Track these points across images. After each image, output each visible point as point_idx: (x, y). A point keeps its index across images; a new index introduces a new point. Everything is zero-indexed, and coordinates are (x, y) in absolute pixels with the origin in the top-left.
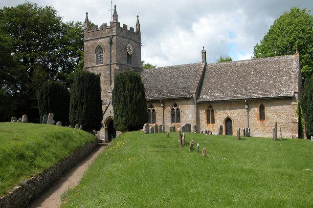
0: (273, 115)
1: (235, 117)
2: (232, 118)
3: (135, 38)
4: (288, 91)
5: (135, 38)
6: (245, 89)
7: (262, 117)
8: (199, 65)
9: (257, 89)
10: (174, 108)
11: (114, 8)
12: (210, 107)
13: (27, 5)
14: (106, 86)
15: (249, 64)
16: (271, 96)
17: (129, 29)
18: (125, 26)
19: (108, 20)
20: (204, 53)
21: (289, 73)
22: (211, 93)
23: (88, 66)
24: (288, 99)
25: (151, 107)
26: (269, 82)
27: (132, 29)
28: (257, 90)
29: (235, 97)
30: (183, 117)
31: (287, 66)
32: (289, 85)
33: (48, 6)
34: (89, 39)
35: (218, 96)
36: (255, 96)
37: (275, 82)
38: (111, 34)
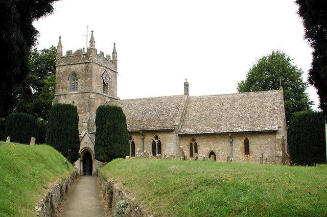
2: (216, 152)
5: (112, 66)
18: (102, 53)
19: (83, 45)
23: (61, 93)
24: (273, 133)
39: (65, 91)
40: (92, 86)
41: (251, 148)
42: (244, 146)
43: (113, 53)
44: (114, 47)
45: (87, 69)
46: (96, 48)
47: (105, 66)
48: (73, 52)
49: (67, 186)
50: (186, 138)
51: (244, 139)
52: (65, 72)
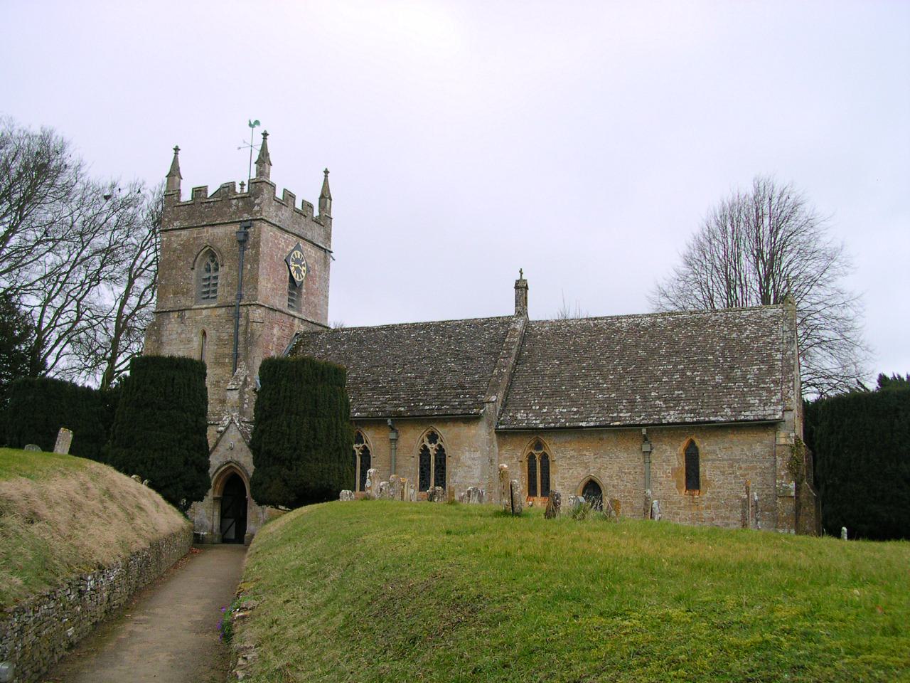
1: (611, 477)
2: (604, 481)
3: (316, 234)
4: (765, 404)
5: (316, 234)
6: (644, 398)
7: (693, 479)
8: (506, 322)
10: (429, 446)
11: (259, 140)
12: (539, 446)
14: (219, 371)
15: (654, 325)
17: (299, 205)
18: (289, 196)
19: (241, 173)
20: (521, 288)
21: (770, 355)
25: (359, 439)
28: (678, 400)
29: (613, 419)
30: (456, 474)
31: (762, 336)
32: (768, 390)
33: (66, 140)
34: (177, 224)
35: (561, 413)
36: (672, 417)
37: (728, 378)
38: (246, 216)
39: (184, 302)
42: (683, 465)
46: (272, 179)
47: (297, 232)
51: (684, 443)
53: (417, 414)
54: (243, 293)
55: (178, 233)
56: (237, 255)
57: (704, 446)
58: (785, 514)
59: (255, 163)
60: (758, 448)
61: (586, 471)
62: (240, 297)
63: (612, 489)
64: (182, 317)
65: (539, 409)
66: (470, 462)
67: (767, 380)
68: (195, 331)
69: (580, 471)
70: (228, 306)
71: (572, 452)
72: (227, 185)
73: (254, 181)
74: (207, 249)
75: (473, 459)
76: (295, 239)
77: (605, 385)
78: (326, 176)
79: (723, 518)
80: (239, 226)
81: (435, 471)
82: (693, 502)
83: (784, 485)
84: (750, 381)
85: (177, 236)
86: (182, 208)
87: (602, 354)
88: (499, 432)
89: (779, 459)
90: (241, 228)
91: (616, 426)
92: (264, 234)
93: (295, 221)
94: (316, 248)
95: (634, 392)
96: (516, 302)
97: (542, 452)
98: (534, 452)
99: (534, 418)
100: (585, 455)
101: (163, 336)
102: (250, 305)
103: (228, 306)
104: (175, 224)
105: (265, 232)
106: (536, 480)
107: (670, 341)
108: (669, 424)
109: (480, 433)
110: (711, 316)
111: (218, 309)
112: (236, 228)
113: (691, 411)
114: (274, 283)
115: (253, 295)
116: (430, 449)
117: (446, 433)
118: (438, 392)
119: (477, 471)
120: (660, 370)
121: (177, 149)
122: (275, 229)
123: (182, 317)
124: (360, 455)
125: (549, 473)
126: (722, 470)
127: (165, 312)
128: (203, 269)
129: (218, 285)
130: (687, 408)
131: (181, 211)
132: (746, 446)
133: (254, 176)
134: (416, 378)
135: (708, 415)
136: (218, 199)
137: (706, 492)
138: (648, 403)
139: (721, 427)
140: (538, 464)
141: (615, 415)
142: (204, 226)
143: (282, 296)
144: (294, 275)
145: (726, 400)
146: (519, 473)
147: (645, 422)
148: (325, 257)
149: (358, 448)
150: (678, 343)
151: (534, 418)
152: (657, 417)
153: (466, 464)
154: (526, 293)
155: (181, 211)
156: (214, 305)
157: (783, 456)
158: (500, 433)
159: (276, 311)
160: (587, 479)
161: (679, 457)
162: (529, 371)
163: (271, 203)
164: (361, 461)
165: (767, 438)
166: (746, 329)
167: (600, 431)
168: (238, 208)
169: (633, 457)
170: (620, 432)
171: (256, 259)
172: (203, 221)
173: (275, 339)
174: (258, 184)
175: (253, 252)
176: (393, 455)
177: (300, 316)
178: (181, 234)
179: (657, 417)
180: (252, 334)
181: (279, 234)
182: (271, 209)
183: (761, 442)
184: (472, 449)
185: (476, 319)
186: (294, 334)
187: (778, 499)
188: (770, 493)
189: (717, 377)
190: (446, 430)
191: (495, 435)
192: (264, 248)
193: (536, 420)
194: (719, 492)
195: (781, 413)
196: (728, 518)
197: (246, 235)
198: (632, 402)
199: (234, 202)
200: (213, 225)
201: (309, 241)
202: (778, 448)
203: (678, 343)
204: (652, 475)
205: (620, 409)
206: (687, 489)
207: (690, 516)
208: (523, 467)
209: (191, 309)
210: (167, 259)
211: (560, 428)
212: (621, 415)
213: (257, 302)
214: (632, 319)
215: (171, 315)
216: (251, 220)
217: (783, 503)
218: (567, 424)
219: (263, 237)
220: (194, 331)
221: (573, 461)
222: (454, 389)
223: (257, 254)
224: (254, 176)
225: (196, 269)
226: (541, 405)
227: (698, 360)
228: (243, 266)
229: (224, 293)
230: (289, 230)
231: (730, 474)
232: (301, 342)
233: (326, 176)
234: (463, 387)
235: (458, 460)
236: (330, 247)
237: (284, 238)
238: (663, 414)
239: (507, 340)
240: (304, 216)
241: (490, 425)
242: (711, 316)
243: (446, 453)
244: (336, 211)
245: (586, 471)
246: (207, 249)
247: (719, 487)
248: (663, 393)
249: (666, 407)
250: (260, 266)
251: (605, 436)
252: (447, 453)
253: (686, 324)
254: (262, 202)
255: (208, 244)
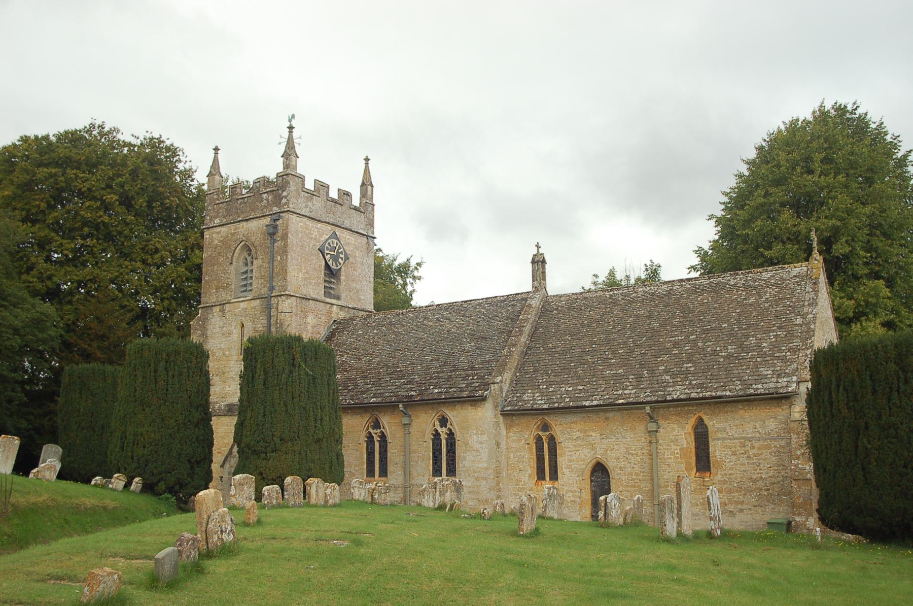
0: (734, 453)
1: (618, 459)
2: (610, 465)
3: (357, 222)
4: (779, 376)
5: (357, 222)
6: (652, 372)
8: (516, 302)
9: (687, 372)
10: (440, 430)
13: (805, 531)
16: (728, 393)
18: (320, 187)
19: (272, 168)
21: (790, 320)
22: (550, 384)
23: (213, 300)
24: (781, 398)
26: (726, 348)
27: (345, 194)
29: (620, 396)
32: (783, 359)
34: (217, 221)
35: (565, 393)
37: (742, 347)
38: (276, 209)
39: (224, 296)
40: (288, 279)
41: (717, 450)
42: (693, 445)
43: (363, 184)
44: (367, 171)
45: (272, 232)
46: (300, 170)
47: (332, 221)
48: (835, 341)
49: (532, 507)
50: (524, 420)
51: (692, 421)
52: (225, 242)
53: (426, 398)
54: (274, 284)
55: (218, 229)
56: (268, 247)
57: (713, 423)
58: (801, 499)
59: (282, 157)
60: (772, 425)
61: (593, 452)
62: (272, 288)
63: (619, 471)
64: (223, 311)
65: (546, 388)
66: (478, 446)
67: (784, 348)
68: (234, 324)
69: (586, 453)
70: (262, 298)
71: (578, 433)
72: (258, 180)
73: (281, 174)
74: (243, 243)
75: (481, 443)
76: (329, 228)
77: (614, 361)
78: (367, 164)
79: (737, 503)
80: (269, 219)
81: (447, 455)
82: (704, 485)
83: (800, 466)
84: (764, 350)
85: (218, 233)
86: (221, 205)
87: (614, 328)
88: (507, 415)
89: (794, 436)
90: (271, 220)
91: (622, 404)
92: (292, 225)
93: (329, 211)
94: (356, 235)
95: (642, 366)
96: (533, 277)
97: (548, 433)
98: (541, 433)
99: (540, 398)
100: (591, 436)
101: (207, 330)
102: (280, 296)
103: (262, 298)
104: (215, 222)
105: (293, 223)
106: (544, 463)
107: (685, 310)
108: (673, 400)
109: (486, 414)
110: (729, 280)
111: (253, 301)
112: (267, 221)
113: (700, 386)
114: (307, 273)
115: (282, 286)
116: (441, 433)
117: (454, 415)
118: (449, 374)
119: (484, 455)
120: (671, 341)
121: (216, 149)
122: (305, 219)
123: (223, 311)
124: (378, 440)
125: (556, 456)
126: (733, 449)
127: (209, 306)
128: (241, 263)
129: (253, 278)
130: (694, 382)
131: (221, 208)
132: (759, 422)
133: (281, 169)
134: (432, 361)
135: (716, 389)
136: (252, 194)
137: (716, 475)
138: (655, 378)
139: (730, 402)
140: (377, 445)
141: (620, 392)
142: (239, 221)
143: (317, 284)
144: (330, 263)
145: (737, 372)
146: (527, 456)
147: (649, 399)
148: (368, 243)
149: (376, 434)
150: (692, 312)
151: (540, 398)
152: (662, 393)
153: (475, 448)
154: (544, 267)
155: (221, 208)
156: (250, 298)
157: (798, 434)
158: (505, 414)
159: (309, 299)
160: (594, 462)
161: (688, 436)
162: (542, 349)
163: (299, 194)
164: (380, 447)
165: (781, 412)
166: (766, 292)
167: (608, 407)
168: (268, 202)
169: (639, 437)
170: (626, 410)
171: (284, 251)
172: (239, 217)
173: (309, 328)
174: (284, 177)
175: (282, 244)
176: (407, 439)
177: (339, 303)
178: (221, 231)
179: (662, 393)
180: (281, 325)
181: (311, 225)
182: (299, 201)
183: (775, 418)
184: (479, 433)
185: (496, 297)
186: (332, 321)
187: (794, 482)
188: (786, 475)
189: (729, 347)
190: (455, 413)
191: (501, 417)
192: (292, 239)
193: (541, 400)
194: (731, 474)
195: (795, 385)
196: (742, 503)
197: (276, 227)
198: (639, 378)
199: (265, 196)
200: (247, 220)
201: (347, 229)
202: (792, 424)
203: (692, 312)
204: (660, 456)
205: (626, 385)
206: (697, 471)
207: (701, 501)
208: (530, 449)
209: (230, 303)
210: (210, 256)
211: (563, 408)
212: (626, 392)
213: (287, 293)
214: (648, 288)
215: (214, 309)
216: (280, 212)
217: (799, 487)
218: (571, 404)
219: (292, 228)
220: (234, 324)
221: (579, 442)
222: (464, 370)
223: (286, 246)
224: (281, 169)
225: (234, 264)
226: (548, 384)
227: (712, 329)
228: (273, 258)
229: (258, 286)
230: (321, 219)
231: (743, 454)
232: (337, 329)
233: (367, 164)
234: (472, 368)
235: (467, 444)
236: (373, 233)
237: (316, 228)
238: (669, 389)
239: (521, 317)
240: (340, 204)
241: (496, 407)
242: (729, 280)
243: (455, 437)
244: (378, 198)
245: (593, 452)
246: (243, 243)
247: (731, 469)
248: (671, 367)
249: (673, 382)
250: (289, 257)
251: (610, 415)
252: (458, 436)
253: (702, 290)
254: (289, 194)
255: (244, 239)
